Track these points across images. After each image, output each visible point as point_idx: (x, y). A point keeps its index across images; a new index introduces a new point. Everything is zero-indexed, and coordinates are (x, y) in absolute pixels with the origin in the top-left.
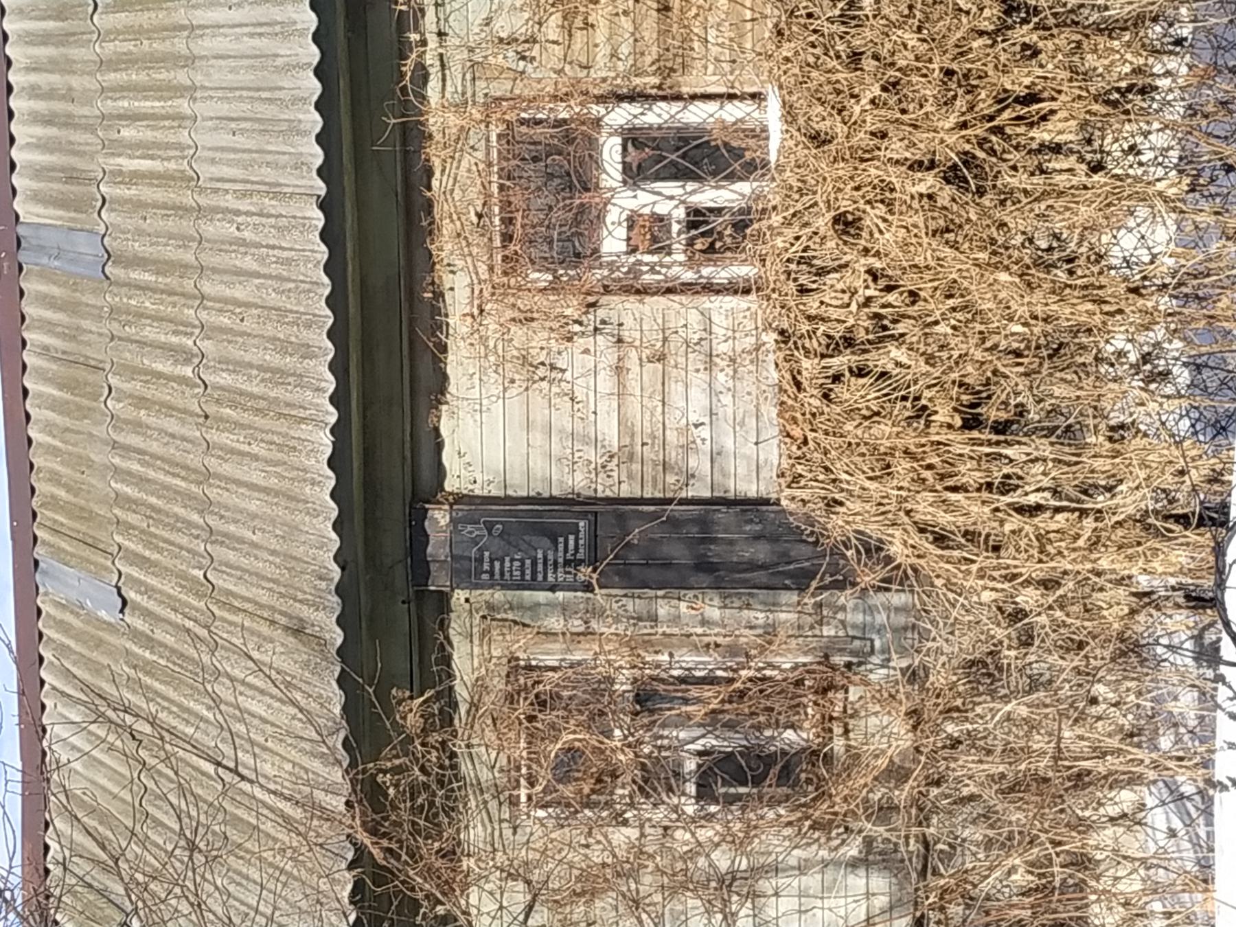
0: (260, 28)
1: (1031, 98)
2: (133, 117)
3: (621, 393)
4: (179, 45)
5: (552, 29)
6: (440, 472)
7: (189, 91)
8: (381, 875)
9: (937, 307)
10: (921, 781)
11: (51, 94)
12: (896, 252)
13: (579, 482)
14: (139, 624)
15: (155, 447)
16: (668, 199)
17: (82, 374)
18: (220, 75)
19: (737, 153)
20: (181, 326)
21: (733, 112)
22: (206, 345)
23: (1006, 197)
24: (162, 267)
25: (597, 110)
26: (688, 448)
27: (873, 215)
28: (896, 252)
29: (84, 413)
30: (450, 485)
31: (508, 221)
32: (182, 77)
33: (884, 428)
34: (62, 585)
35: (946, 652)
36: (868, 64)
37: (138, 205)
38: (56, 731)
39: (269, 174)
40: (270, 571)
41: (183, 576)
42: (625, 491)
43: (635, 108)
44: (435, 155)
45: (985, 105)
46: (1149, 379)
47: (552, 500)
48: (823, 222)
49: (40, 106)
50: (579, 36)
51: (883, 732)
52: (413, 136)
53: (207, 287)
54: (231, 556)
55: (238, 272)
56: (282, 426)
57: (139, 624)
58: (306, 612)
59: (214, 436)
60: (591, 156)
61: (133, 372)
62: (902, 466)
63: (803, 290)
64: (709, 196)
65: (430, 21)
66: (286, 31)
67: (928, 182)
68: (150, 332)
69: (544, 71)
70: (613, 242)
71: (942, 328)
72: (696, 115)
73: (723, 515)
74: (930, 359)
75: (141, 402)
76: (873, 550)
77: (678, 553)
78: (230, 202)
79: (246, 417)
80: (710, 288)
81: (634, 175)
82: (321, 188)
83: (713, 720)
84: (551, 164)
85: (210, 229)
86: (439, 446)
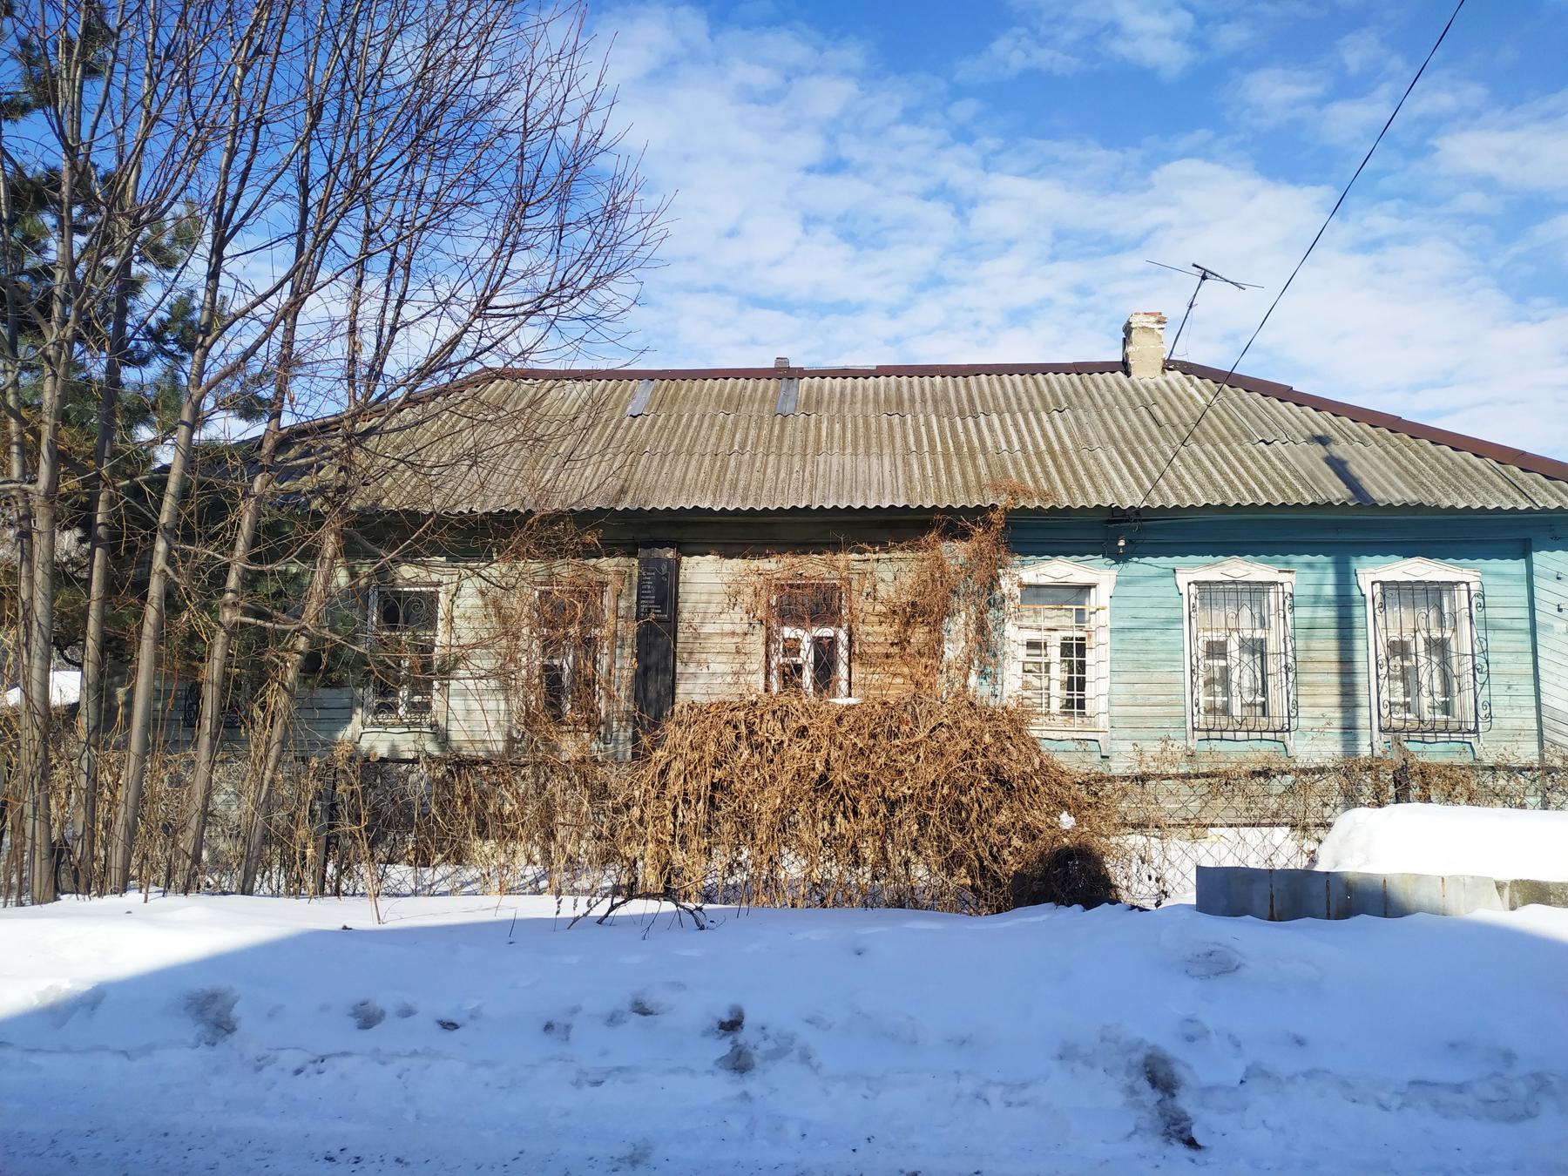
0: (881, 484)
1: (855, 813)
2: (844, 429)
3: (723, 634)
4: (874, 450)
5: (879, 608)
6: (690, 555)
7: (855, 453)
8: (521, 523)
9: (766, 772)
10: (547, 767)
11: (853, 395)
12: (790, 753)
13: (685, 615)
14: (625, 423)
15: (703, 433)
16: (806, 656)
17: (735, 402)
18: (862, 466)
19: (827, 686)
20: (755, 446)
21: (843, 685)
22: (747, 456)
23: (813, 802)
24: (780, 439)
25: (845, 626)
26: (699, 663)
27: (806, 743)
28: (790, 753)
29: (718, 403)
30: (685, 559)
31: (798, 587)
32: (861, 450)
33: (713, 748)
34: (643, 390)
35: (613, 777)
36: (871, 742)
37: (807, 430)
38: (579, 385)
39: (820, 485)
40: (649, 480)
41: (647, 442)
42: (680, 635)
43: (846, 642)
44: (827, 556)
45: (852, 793)
46: (730, 866)
47: (677, 603)
48: (804, 721)
49: (848, 390)
50: (876, 619)
51: (569, 748)
52: (836, 547)
53: (772, 458)
54: (655, 463)
55: (778, 471)
56: (712, 487)
57: (625, 423)
58: (630, 495)
59: (708, 458)
60: (119, 521)
61: (736, 424)
62: (696, 755)
63: (774, 712)
64: (807, 676)
65: (883, 556)
66: (881, 495)
67: (820, 767)
68: (752, 433)
69: (861, 604)
70: (788, 632)
71: (756, 774)
72: (842, 670)
73: (669, 678)
74: (744, 768)
75: (722, 428)
76: (657, 743)
77: (654, 657)
78: (808, 468)
79: (716, 472)
80: (768, 674)
81: (817, 642)
82: (814, 507)
83: (576, 671)
84: (822, 605)
85: (797, 459)
86: (701, 555)
